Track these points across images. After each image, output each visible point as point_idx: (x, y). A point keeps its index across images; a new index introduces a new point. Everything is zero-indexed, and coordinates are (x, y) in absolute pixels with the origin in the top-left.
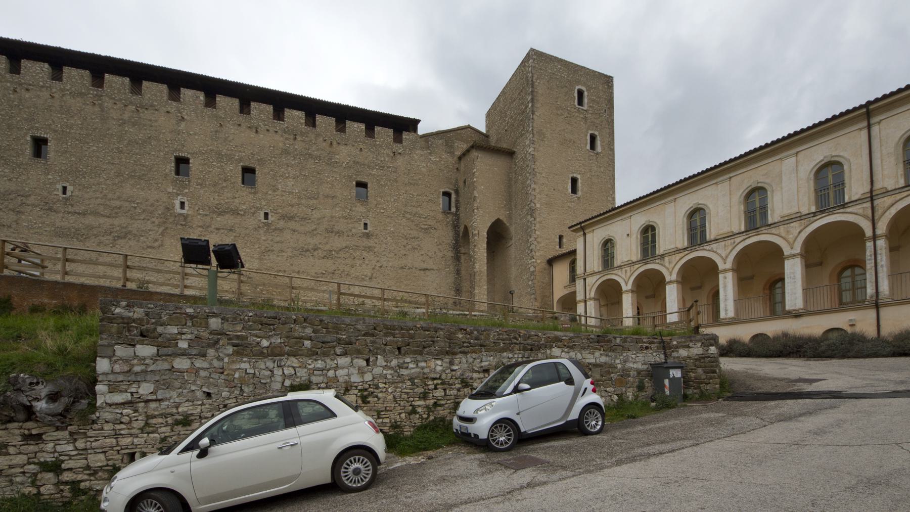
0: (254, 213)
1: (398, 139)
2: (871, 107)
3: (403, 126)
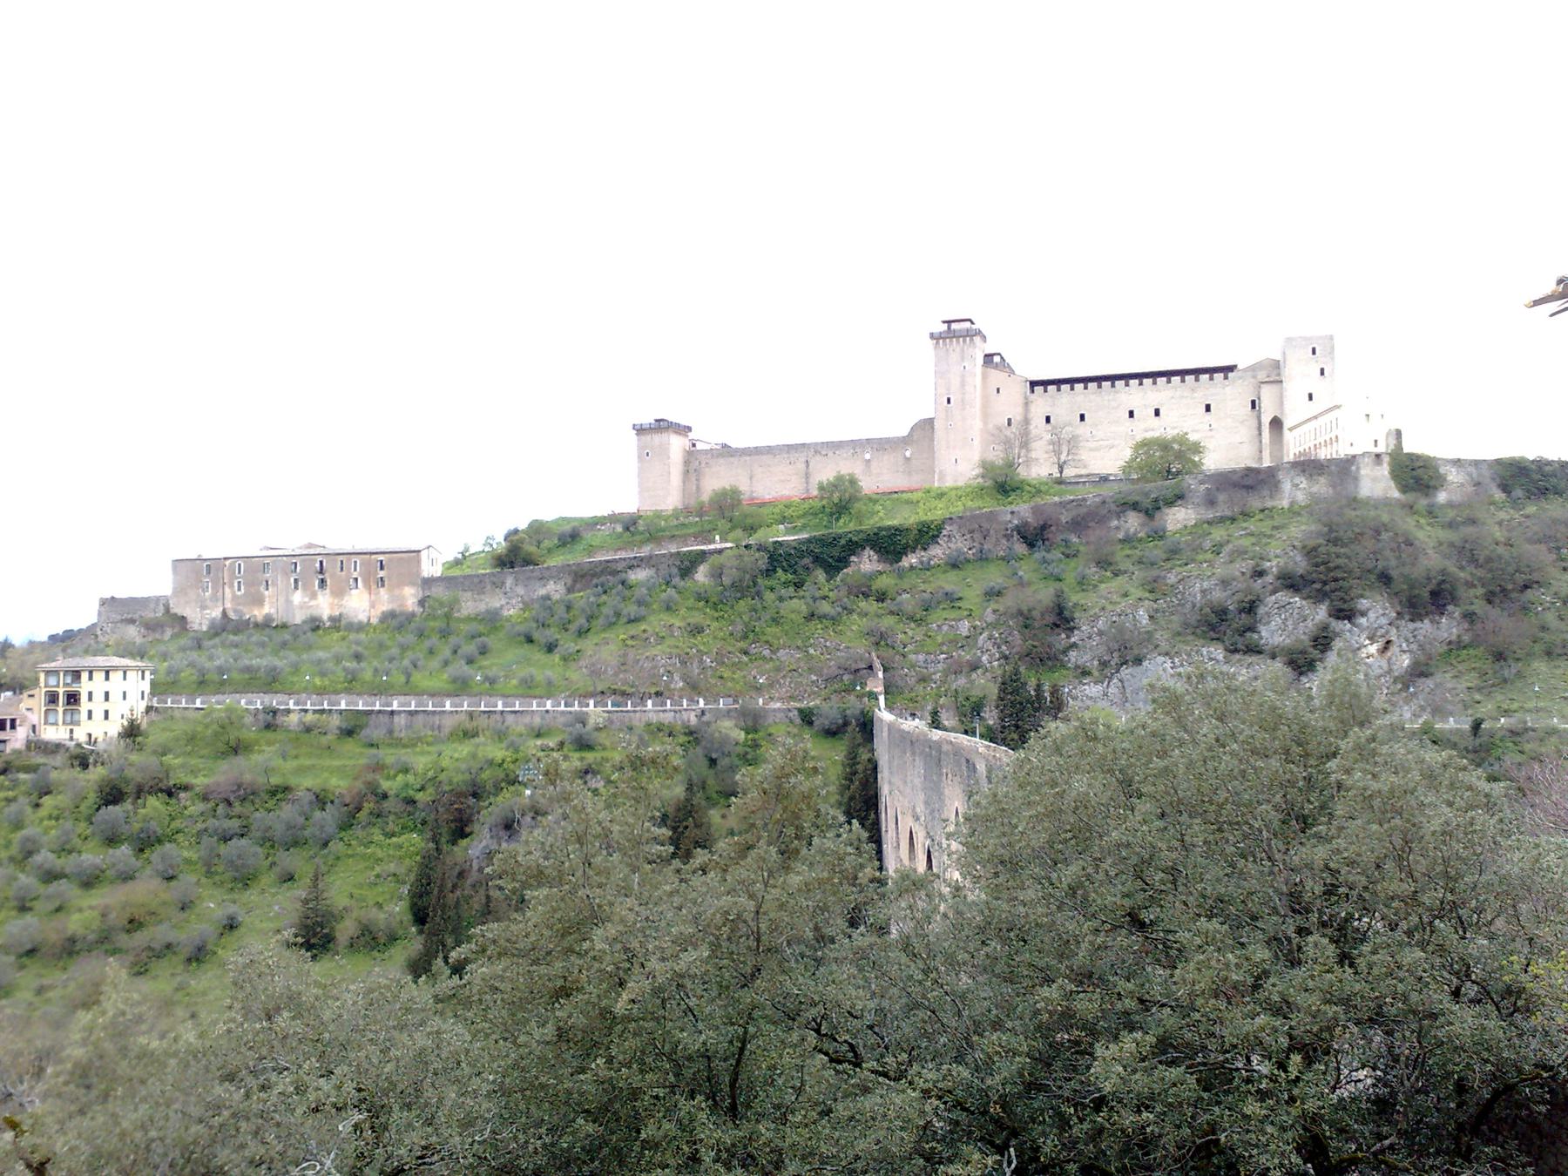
0: (1236, 651)
1: (1226, 378)
2: (954, 326)
3: (1227, 370)
